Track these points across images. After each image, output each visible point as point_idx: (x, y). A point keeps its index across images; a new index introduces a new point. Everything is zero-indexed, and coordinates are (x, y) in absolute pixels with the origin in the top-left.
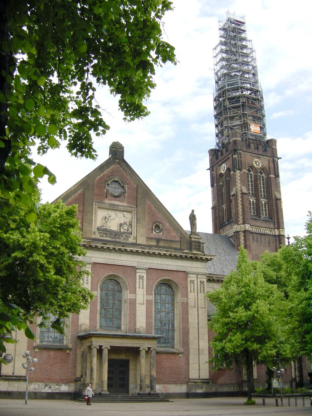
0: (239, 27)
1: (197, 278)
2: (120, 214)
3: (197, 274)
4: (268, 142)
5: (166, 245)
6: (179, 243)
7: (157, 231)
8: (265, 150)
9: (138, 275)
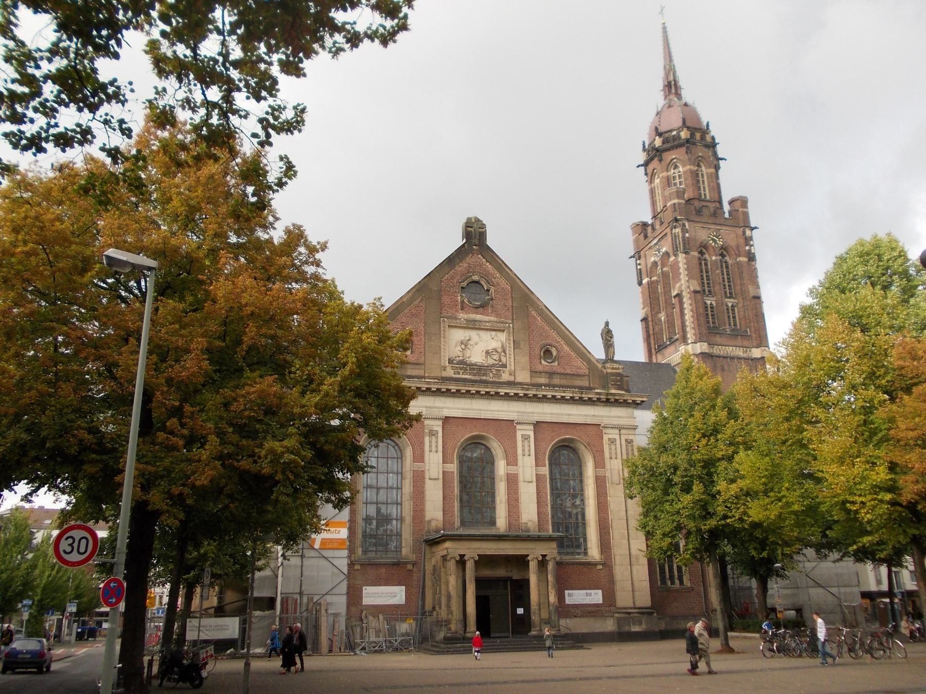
2: (485, 335)
3: (620, 428)
5: (564, 382)
9: (519, 434)
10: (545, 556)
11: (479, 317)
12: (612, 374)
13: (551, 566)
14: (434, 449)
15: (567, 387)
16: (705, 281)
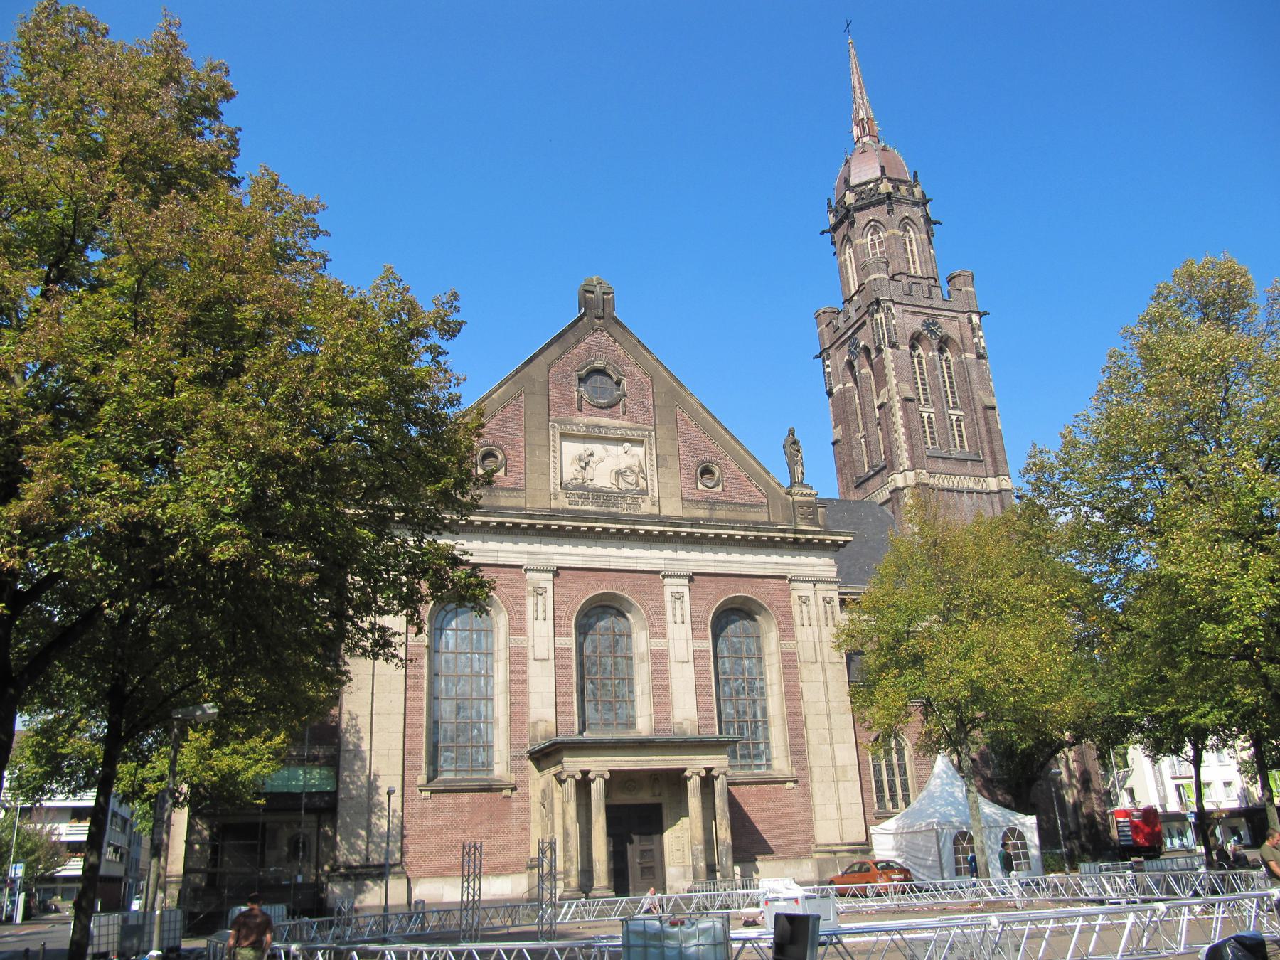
9: (668, 591)
10: (711, 769)
12: (802, 504)
14: (541, 616)
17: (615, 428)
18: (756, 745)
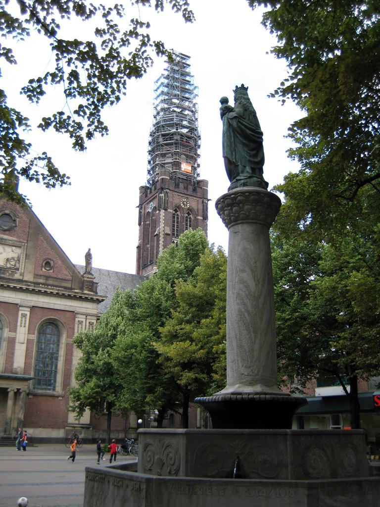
0: (184, 61)
1: (86, 319)
2: (8, 249)
3: (87, 315)
4: (199, 182)
5: (55, 283)
6: (70, 282)
7: (48, 269)
8: (194, 190)
9: (20, 312)
11: (5, 237)
12: (87, 281)
13: (23, 395)
14: (23, 325)
15: (56, 286)
16: (176, 228)
17: (10, 240)
18: (50, 380)
